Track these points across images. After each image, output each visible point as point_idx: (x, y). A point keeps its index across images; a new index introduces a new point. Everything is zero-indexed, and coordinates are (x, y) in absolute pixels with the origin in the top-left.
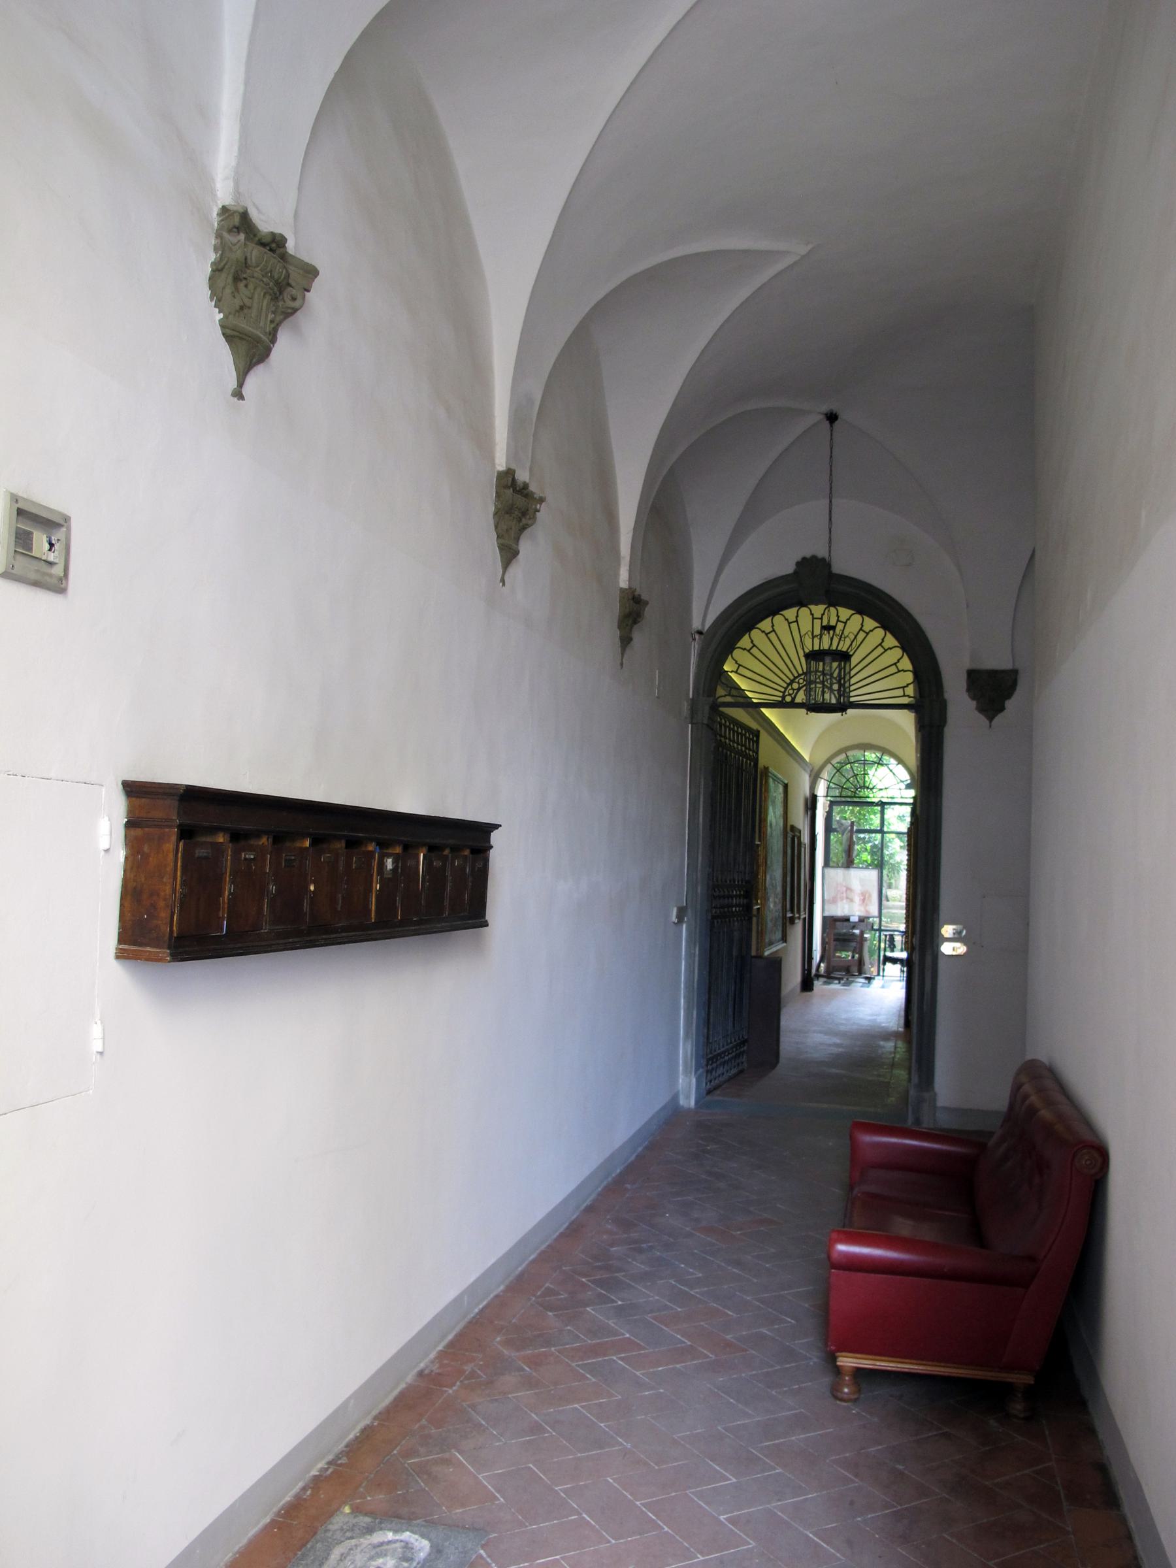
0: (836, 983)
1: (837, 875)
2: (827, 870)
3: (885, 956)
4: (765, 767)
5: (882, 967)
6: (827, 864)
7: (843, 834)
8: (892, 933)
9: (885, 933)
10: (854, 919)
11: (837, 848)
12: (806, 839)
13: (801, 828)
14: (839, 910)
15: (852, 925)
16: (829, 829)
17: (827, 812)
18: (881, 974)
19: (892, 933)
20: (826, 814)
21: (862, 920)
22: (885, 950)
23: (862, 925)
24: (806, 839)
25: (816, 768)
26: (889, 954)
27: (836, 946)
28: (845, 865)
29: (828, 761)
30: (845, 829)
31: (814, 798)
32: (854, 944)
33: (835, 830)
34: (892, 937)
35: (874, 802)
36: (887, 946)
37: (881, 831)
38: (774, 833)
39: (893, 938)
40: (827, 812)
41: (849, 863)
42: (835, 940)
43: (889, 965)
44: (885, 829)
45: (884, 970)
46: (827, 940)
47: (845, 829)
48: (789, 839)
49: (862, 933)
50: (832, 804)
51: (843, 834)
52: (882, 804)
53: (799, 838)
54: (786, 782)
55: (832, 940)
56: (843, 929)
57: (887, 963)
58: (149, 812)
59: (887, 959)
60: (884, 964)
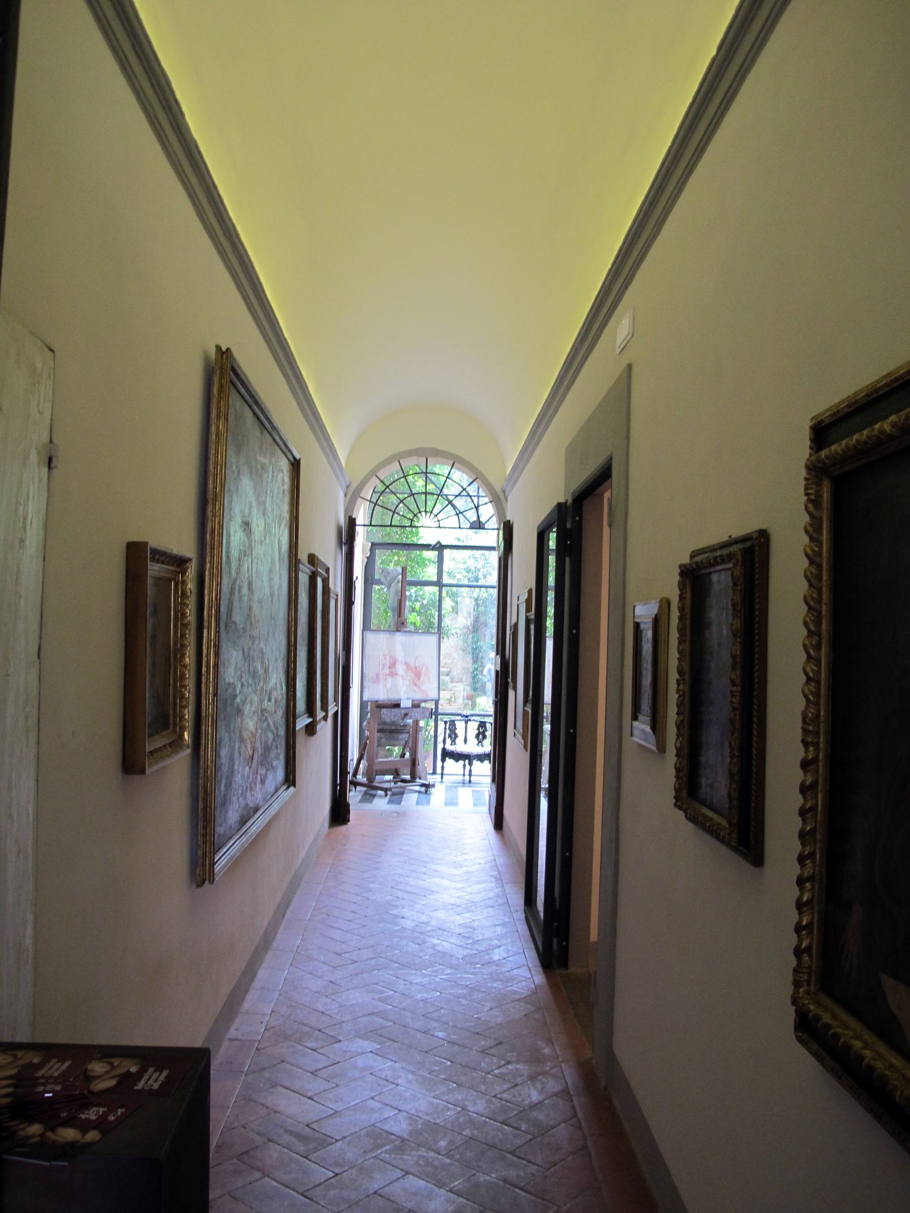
0: (381, 796)
1: (379, 642)
2: (370, 636)
3: (444, 750)
4: (218, 348)
5: (439, 763)
6: (366, 627)
7: (389, 587)
8: (453, 718)
9: (447, 718)
10: (406, 703)
11: (382, 612)
12: (337, 585)
13: (330, 564)
14: (379, 692)
15: (403, 712)
16: (369, 581)
17: (367, 558)
18: (439, 770)
19: (453, 718)
20: (366, 560)
21: (416, 705)
22: (444, 742)
23: (416, 713)
24: (337, 585)
25: (354, 485)
26: (449, 747)
27: (380, 739)
28: (393, 627)
29: (373, 473)
30: (393, 579)
31: (352, 523)
32: (405, 736)
33: (379, 582)
34: (453, 723)
35: (430, 545)
36: (447, 736)
37: (439, 584)
38: (258, 551)
39: (455, 725)
40: (367, 558)
41: (400, 625)
42: (379, 731)
43: (449, 762)
44: (446, 580)
45: (443, 768)
46: (367, 733)
47: (393, 579)
48: (304, 579)
49: (416, 722)
50: (374, 546)
51: (389, 587)
52: (440, 548)
53: (326, 581)
54: (298, 456)
55: (376, 730)
56: (388, 715)
57: (447, 759)
58: (250, 637)
59: (446, 754)
60: (443, 760)
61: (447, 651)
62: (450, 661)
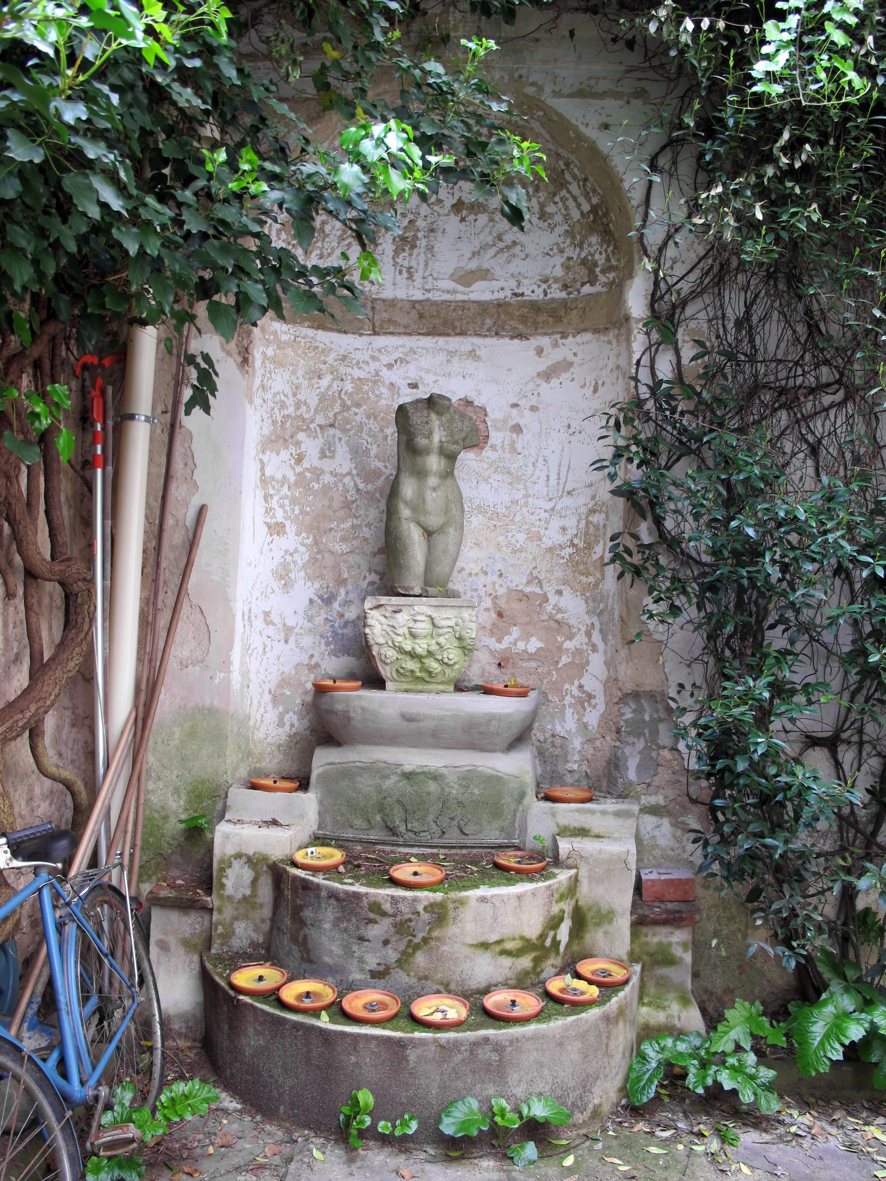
61: (518, 580)
62: (534, 645)
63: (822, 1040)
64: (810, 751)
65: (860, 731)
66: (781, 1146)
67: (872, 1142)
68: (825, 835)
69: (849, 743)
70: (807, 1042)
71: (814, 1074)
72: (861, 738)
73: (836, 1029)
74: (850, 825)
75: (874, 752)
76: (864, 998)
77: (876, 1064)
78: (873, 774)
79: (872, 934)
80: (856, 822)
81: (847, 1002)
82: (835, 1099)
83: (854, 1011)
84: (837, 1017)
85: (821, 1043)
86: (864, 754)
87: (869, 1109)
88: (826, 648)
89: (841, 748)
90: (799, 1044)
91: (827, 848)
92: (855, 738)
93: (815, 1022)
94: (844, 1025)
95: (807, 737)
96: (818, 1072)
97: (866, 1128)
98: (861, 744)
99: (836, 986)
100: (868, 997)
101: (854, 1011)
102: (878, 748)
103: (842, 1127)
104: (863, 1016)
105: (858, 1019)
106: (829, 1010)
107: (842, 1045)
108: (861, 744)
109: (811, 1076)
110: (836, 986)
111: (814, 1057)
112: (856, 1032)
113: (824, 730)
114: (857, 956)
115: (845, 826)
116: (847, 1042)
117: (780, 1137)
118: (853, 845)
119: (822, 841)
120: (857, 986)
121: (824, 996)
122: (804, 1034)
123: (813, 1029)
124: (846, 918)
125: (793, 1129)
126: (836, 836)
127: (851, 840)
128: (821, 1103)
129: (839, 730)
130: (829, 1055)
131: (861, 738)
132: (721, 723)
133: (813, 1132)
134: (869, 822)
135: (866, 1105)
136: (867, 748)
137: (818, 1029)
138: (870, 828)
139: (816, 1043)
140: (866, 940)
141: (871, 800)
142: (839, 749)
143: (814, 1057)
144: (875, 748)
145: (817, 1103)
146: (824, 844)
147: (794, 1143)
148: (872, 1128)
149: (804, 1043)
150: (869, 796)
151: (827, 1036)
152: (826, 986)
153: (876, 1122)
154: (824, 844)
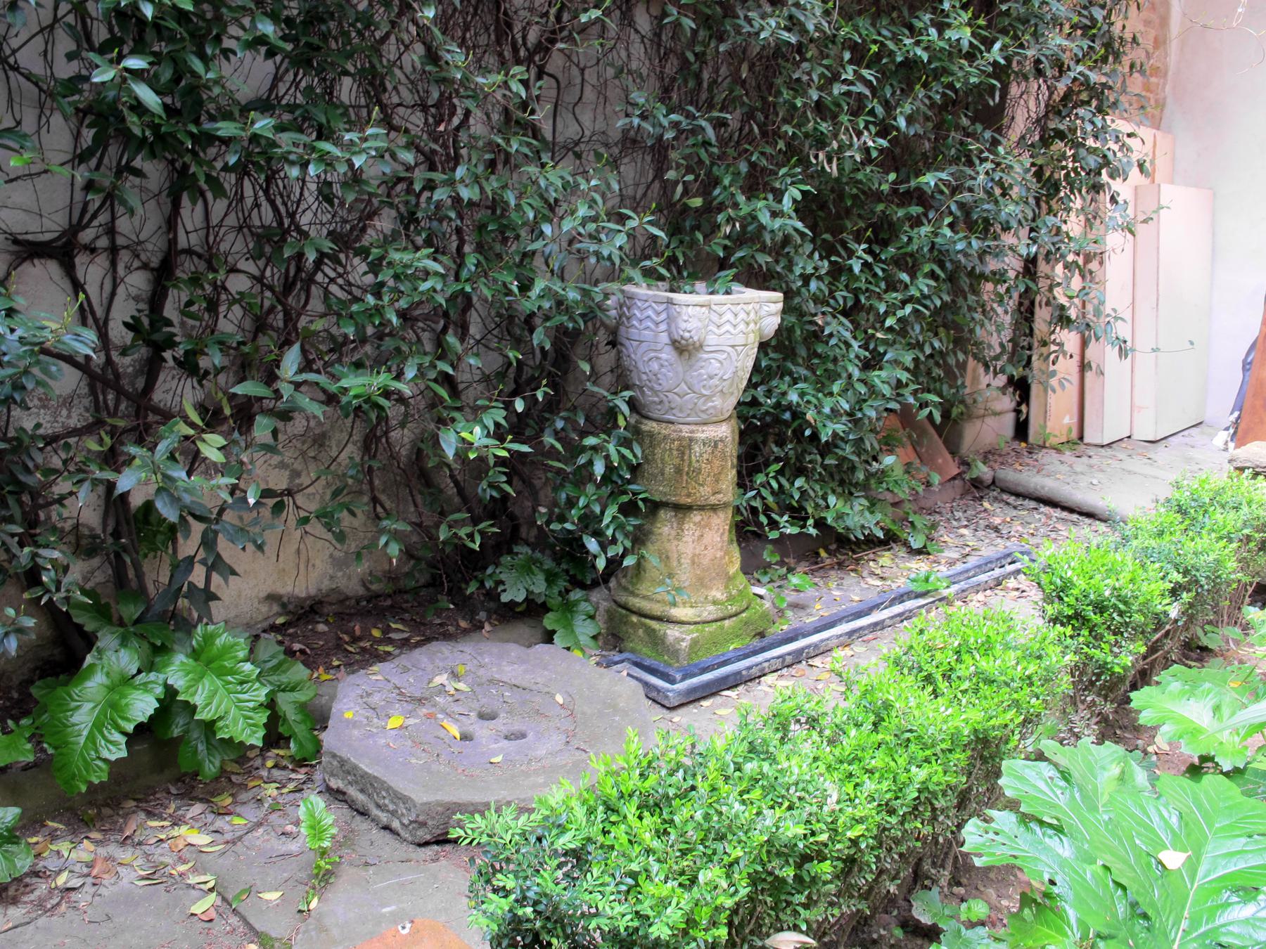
63: (91, 732)
64: (26, 266)
65: (111, 231)
66: (42, 921)
67: (186, 854)
68: (68, 402)
69: (93, 250)
70: (67, 743)
71: (84, 788)
72: (113, 241)
73: (113, 708)
74: (107, 384)
75: (136, 264)
76: (153, 645)
77: (180, 739)
78: (137, 299)
79: (160, 538)
80: (117, 376)
81: (127, 660)
82: (126, 797)
83: (139, 672)
84: (111, 689)
85: (91, 738)
86: (121, 271)
87: (180, 796)
88: (36, 84)
89: (80, 260)
90: (56, 748)
91: (74, 422)
92: (103, 242)
93: (78, 707)
94: (124, 702)
95: (16, 242)
96: (90, 784)
97: (176, 832)
98: (113, 251)
99: (107, 639)
100: (159, 643)
101: (139, 672)
102: (143, 257)
103: (140, 843)
104: (152, 676)
105: (145, 684)
106: (94, 685)
107: (124, 733)
108: (113, 251)
109: (80, 793)
110: (107, 639)
111: (80, 764)
112: (143, 706)
113: (50, 227)
114: (140, 576)
115: (99, 385)
116: (130, 727)
117: (40, 904)
118: (114, 415)
119: (64, 412)
120: (140, 628)
121: (89, 659)
122: (60, 732)
123: (76, 718)
124: (118, 523)
125: (61, 880)
126: (87, 402)
127: (111, 404)
128: (106, 811)
129: (75, 229)
130: (105, 754)
131: (113, 241)
132: (699, 471)
133: (95, 872)
134: (137, 373)
135: (174, 791)
136: (124, 257)
137: (82, 717)
138: (140, 383)
139: (82, 740)
140: (151, 550)
141: (134, 340)
142: (78, 260)
143: (80, 764)
144: (138, 256)
145: (99, 813)
146: (69, 417)
147: (64, 906)
148: (183, 830)
149: (62, 744)
150: (131, 335)
151: (98, 726)
152: (89, 641)
153: (189, 815)
154: (69, 417)
